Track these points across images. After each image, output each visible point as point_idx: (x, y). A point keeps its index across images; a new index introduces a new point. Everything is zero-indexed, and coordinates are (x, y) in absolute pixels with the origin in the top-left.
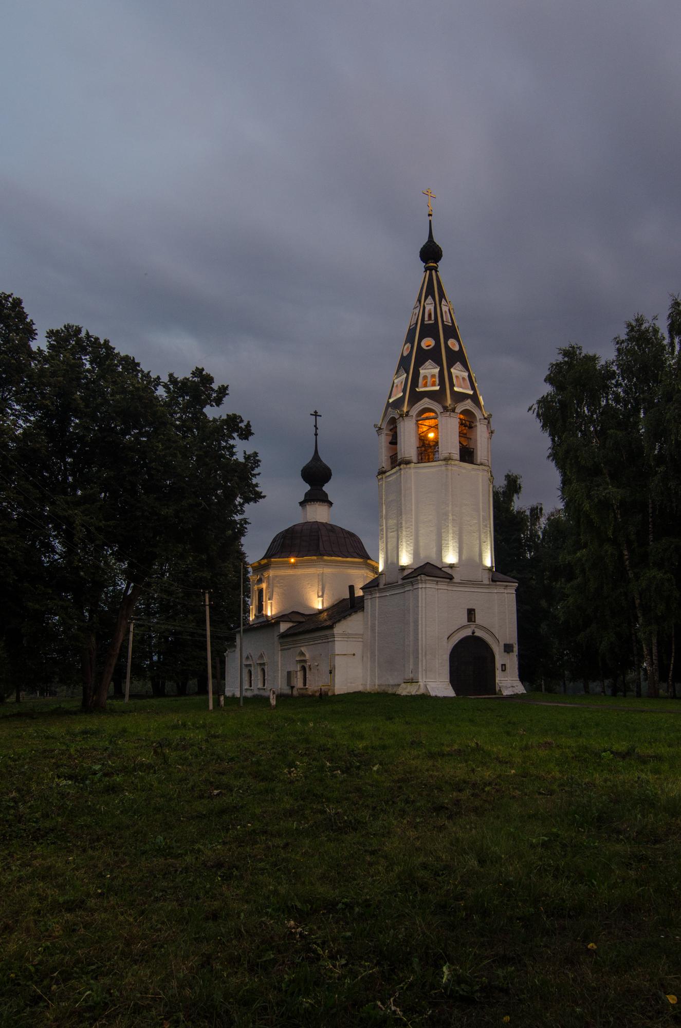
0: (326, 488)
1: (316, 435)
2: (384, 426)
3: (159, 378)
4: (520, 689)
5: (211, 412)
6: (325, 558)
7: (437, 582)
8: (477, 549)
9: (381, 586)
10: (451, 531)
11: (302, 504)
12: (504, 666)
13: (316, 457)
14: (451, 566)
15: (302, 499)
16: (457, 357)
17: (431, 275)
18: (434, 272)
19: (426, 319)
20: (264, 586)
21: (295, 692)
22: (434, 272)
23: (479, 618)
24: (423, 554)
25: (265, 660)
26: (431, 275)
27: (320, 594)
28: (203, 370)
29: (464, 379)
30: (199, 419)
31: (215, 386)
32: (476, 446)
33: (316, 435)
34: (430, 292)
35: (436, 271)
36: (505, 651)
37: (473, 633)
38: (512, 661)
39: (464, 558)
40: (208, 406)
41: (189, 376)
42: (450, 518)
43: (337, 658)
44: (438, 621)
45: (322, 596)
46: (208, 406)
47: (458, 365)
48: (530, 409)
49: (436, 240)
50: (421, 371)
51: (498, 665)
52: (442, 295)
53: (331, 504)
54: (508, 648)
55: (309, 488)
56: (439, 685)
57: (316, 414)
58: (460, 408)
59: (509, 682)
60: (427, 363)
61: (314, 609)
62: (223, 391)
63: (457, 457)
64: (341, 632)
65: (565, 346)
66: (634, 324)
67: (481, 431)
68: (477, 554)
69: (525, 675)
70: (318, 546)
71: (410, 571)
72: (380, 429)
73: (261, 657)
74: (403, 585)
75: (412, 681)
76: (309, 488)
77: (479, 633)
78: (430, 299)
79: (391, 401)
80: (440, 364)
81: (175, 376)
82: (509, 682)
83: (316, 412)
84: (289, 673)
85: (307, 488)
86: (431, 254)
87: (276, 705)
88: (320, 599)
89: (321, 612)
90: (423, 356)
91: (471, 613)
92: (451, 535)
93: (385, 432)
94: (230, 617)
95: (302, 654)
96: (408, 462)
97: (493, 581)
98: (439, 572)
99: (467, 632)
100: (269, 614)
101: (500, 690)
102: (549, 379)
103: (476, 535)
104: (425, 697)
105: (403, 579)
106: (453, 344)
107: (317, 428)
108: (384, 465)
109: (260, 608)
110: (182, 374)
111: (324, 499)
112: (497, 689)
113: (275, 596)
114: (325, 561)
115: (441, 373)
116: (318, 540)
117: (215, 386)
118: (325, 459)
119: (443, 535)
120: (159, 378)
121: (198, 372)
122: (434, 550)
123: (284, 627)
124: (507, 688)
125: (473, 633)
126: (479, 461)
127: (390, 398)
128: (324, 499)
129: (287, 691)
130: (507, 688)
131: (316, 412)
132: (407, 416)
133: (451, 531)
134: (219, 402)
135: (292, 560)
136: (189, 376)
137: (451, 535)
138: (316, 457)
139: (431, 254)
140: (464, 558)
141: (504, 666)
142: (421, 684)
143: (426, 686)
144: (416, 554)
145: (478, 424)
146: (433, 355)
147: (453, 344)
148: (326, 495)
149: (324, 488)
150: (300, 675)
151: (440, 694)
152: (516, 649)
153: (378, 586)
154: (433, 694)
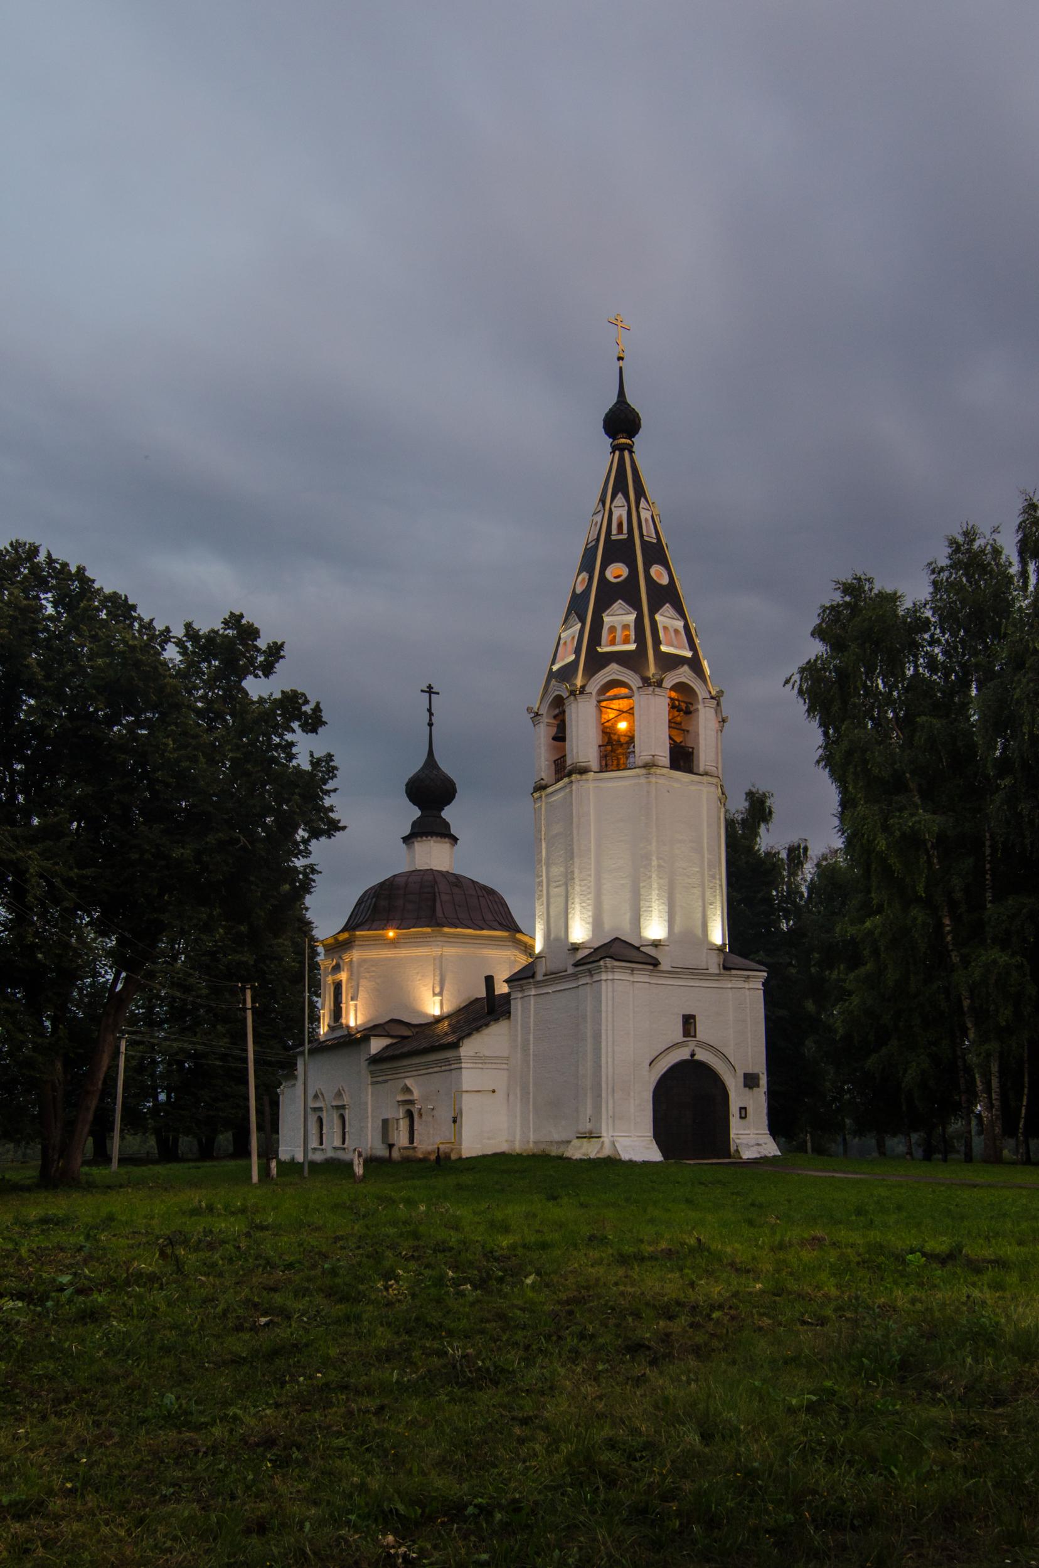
0: (447, 813)
1: (430, 725)
2: (544, 711)
3: (168, 630)
4: (771, 1148)
5: (256, 687)
6: (446, 930)
7: (633, 970)
8: (699, 915)
9: (539, 977)
10: (655, 886)
11: (407, 840)
12: (743, 1110)
13: (431, 761)
14: (656, 944)
15: (407, 831)
16: (666, 596)
17: (622, 459)
18: (626, 453)
19: (614, 531)
20: (343, 976)
21: (396, 1154)
22: (626, 453)
23: (703, 1031)
24: (608, 924)
25: (346, 1100)
26: (622, 459)
27: (437, 990)
28: (242, 616)
29: (676, 631)
30: (235, 697)
31: (262, 644)
32: (698, 743)
33: (430, 725)
34: (620, 486)
35: (631, 452)
36: (745, 1086)
37: (693, 1055)
38: (757, 1102)
39: (677, 930)
40: (250, 678)
41: (218, 626)
42: (655, 863)
43: (465, 1096)
44: (632, 1036)
45: (441, 994)
46: (250, 678)
47: (667, 608)
48: (787, 682)
49: (630, 400)
50: (606, 619)
51: (734, 1109)
52: (640, 493)
53: (455, 840)
54: (750, 1081)
55: (418, 813)
56: (633, 1140)
57: (430, 691)
58: (671, 679)
59: (751, 1137)
60: (615, 606)
61: (426, 1015)
62: (276, 651)
63: (666, 761)
64: (471, 1053)
65: (847, 577)
66: (960, 539)
67: (705, 719)
68: (699, 923)
69: (778, 1126)
70: (434, 910)
71: (587, 952)
72: (537, 714)
73: (339, 1094)
74: (575, 976)
75: (590, 1136)
76: (418, 813)
77: (702, 1056)
78: (620, 499)
79: (555, 668)
80: (637, 606)
81: (196, 626)
82: (751, 1137)
83: (430, 687)
84: (385, 1122)
85: (416, 813)
86: (622, 423)
87: (364, 1176)
88: (438, 998)
89: (438, 1020)
90: (608, 594)
91: (689, 1022)
92: (655, 893)
93: (545, 719)
94: (287, 1031)
95: (407, 1090)
96: (583, 771)
97: (726, 968)
98: (634, 953)
99: (683, 1054)
100: (352, 1024)
101: (737, 1151)
102: (819, 633)
103: (697, 892)
104: (612, 1163)
105: (576, 965)
106: (659, 574)
107: (431, 714)
108: (543, 775)
109: (337, 1013)
110: (209, 623)
111: (444, 832)
112: (733, 1148)
113: (362, 994)
114: (445, 935)
115: (639, 621)
116: (434, 901)
117: (262, 644)
118: (447, 766)
119: (643, 891)
120: (168, 630)
121: (234, 620)
122: (628, 917)
123: (377, 1045)
124: (748, 1146)
125: (693, 1055)
126: (701, 770)
127: (553, 663)
128: (444, 832)
129: (381, 1151)
130: (748, 1146)
131: (430, 687)
132: (581, 693)
133: (655, 886)
134: (268, 669)
135: (391, 934)
136: (218, 626)
137: (655, 893)
138: (431, 761)
139: (622, 423)
140: (677, 930)
141: (743, 1110)
142: (606, 1140)
143: (613, 1143)
144: (597, 924)
145: (700, 707)
146: (627, 592)
147: (659, 574)
148: (447, 825)
149: (444, 814)
150: (403, 1125)
151: (638, 1157)
152: (763, 1081)
153: (533, 976)
154: (625, 1156)
